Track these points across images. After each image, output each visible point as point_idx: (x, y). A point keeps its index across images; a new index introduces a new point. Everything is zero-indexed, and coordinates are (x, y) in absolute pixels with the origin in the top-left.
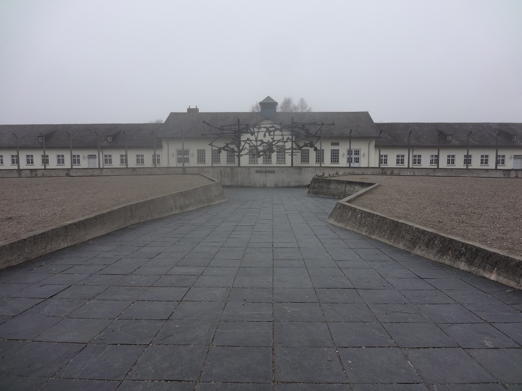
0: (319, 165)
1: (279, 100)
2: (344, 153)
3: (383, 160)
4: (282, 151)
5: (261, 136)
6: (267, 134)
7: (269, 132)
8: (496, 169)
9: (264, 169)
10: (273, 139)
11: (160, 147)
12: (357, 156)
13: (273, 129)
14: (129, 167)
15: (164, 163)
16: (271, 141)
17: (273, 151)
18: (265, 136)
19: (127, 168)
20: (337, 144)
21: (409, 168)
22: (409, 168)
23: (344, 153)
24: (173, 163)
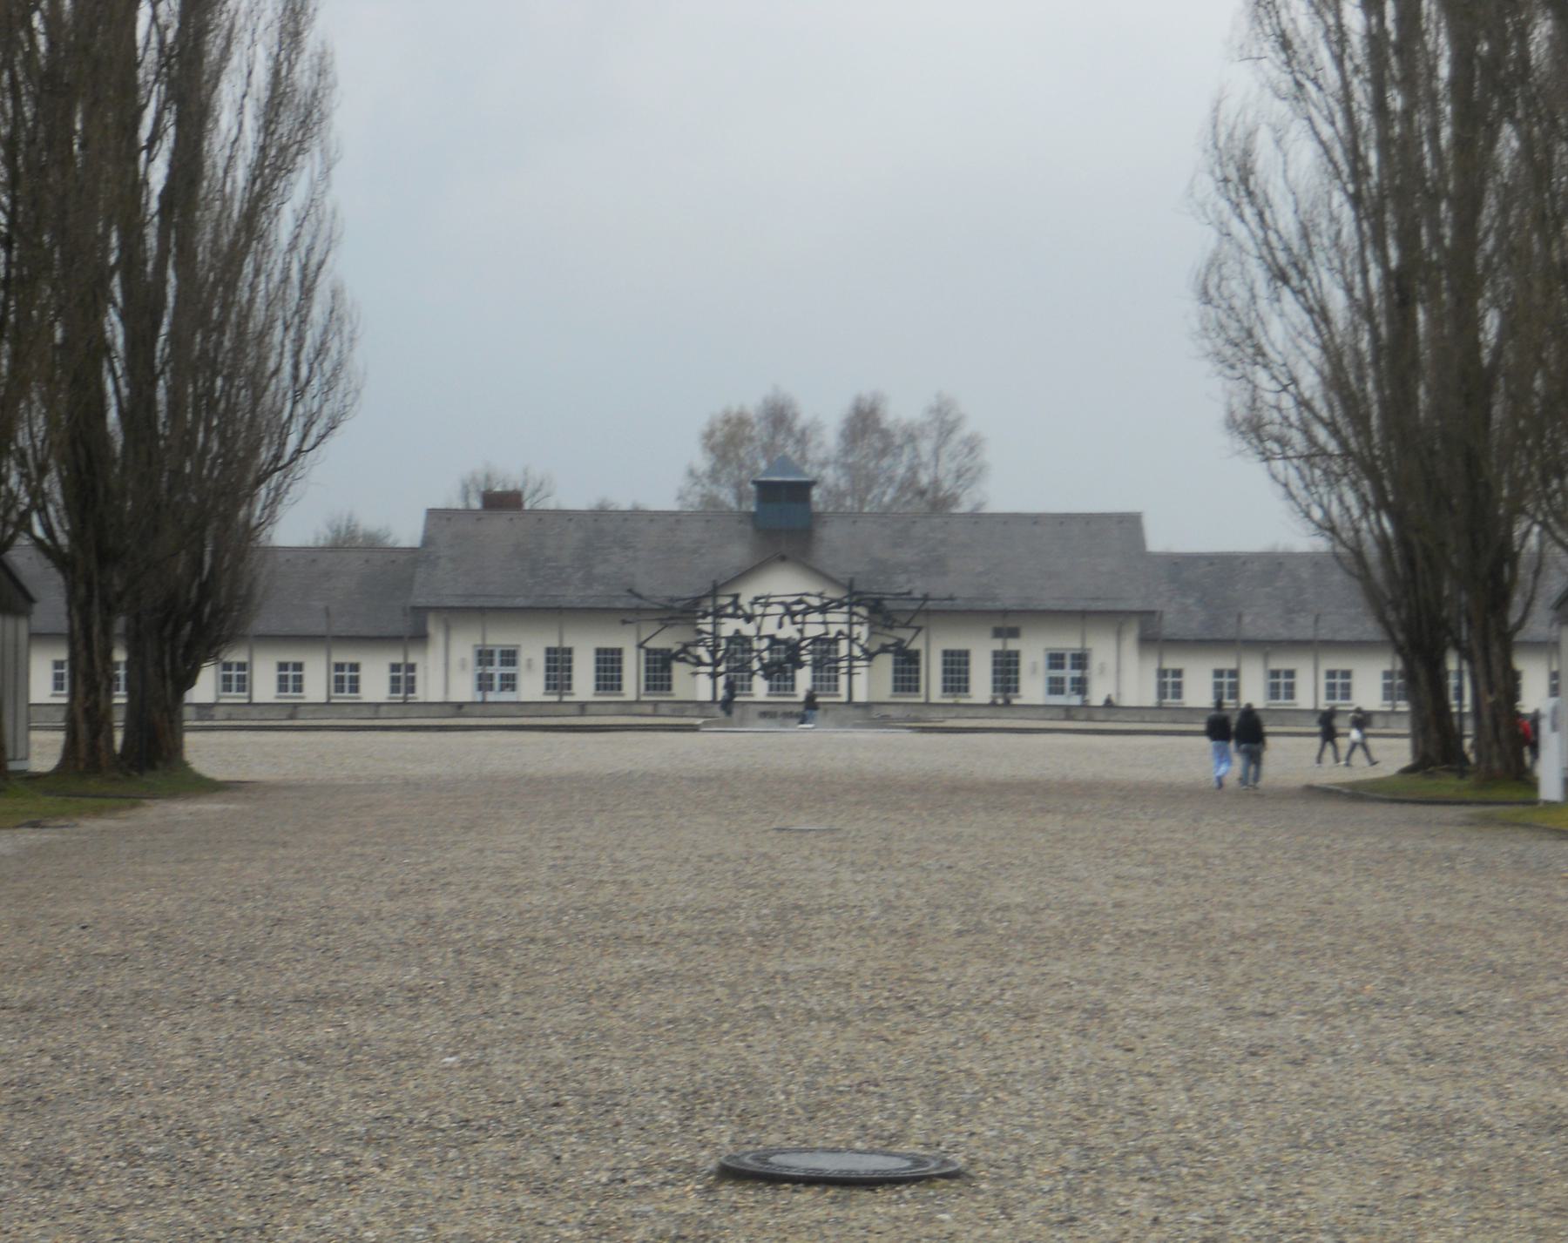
0: (555, 698)
1: (823, 412)
2: (1035, 664)
3: (1170, 683)
4: (825, 655)
5: (770, 626)
6: (787, 619)
7: (793, 615)
8: (1160, 707)
9: (780, 709)
10: (801, 631)
11: (419, 638)
12: (508, 670)
13: (801, 607)
14: (256, 700)
15: (430, 688)
16: (797, 636)
17: (801, 665)
18: (780, 625)
19: (250, 704)
20: (1014, 633)
21: (850, 702)
22: (850, 702)
23: (1035, 664)
24: (464, 689)
